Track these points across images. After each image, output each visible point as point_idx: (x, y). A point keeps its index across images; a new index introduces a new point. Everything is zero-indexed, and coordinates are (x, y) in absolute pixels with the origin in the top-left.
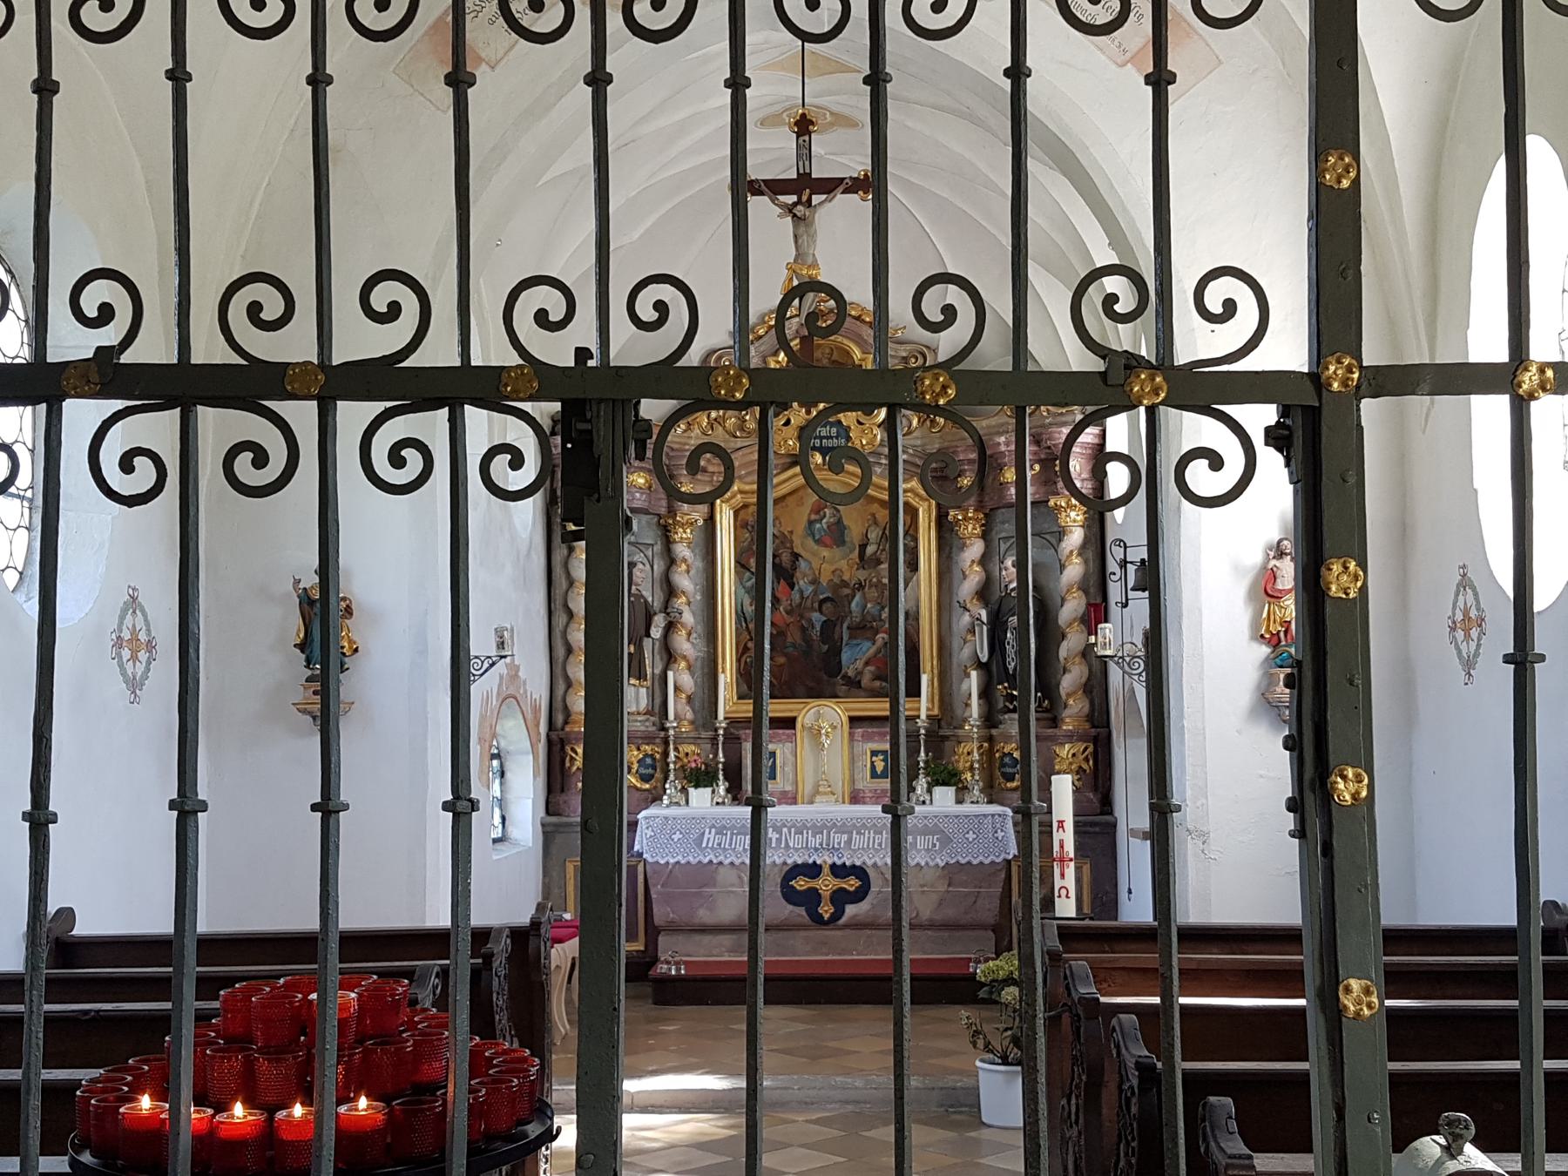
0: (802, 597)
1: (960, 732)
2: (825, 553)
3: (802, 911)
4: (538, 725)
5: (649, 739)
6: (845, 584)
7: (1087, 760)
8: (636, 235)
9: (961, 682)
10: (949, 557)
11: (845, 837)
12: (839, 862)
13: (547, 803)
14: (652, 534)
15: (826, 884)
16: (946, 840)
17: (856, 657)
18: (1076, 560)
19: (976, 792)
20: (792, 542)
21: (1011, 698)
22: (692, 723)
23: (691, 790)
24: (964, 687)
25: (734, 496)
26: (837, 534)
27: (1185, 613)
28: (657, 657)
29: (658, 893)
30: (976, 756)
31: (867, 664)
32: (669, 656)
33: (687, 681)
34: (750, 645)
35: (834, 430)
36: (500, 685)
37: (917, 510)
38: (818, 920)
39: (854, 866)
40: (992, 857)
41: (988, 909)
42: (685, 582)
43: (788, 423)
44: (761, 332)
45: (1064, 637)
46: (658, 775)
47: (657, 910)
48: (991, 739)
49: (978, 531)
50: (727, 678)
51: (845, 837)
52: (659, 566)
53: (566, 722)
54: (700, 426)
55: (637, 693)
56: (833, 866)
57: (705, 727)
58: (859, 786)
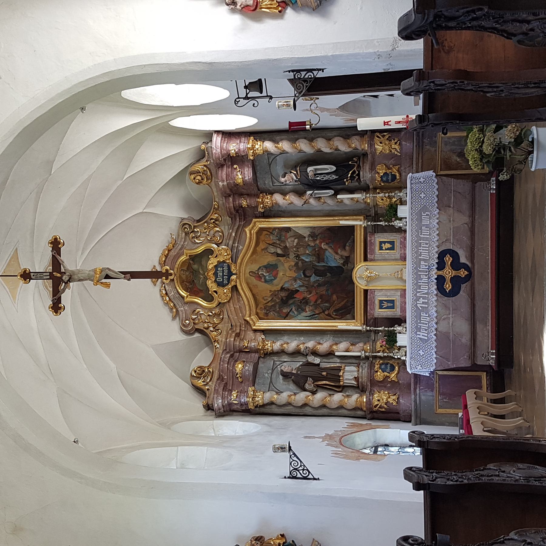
1: (371, 204)
2: (281, 274)
3: (463, 286)
4: (361, 425)
5: (372, 366)
6: (296, 264)
7: (383, 136)
8: (113, 365)
9: (345, 204)
10: (284, 212)
11: (422, 263)
12: (436, 266)
13: (405, 421)
14: (268, 362)
15: (448, 273)
16: (425, 209)
17: (333, 259)
19: (401, 194)
20: (275, 291)
21: (352, 178)
23: (398, 344)
24: (347, 202)
25: (253, 321)
26: (272, 268)
27: (267, 57)
28: (331, 360)
31: (337, 253)
32: (330, 354)
33: (343, 345)
34: (326, 313)
35: (219, 269)
38: (469, 277)
39: (438, 258)
41: (464, 186)
42: (292, 345)
43: (216, 292)
44: (172, 304)
45: (319, 151)
46: (391, 362)
47: (463, 365)
48: (375, 189)
50: (342, 325)
51: (422, 263)
52: (285, 358)
53: (362, 410)
56: (438, 269)
57: (369, 337)
58: (398, 256)
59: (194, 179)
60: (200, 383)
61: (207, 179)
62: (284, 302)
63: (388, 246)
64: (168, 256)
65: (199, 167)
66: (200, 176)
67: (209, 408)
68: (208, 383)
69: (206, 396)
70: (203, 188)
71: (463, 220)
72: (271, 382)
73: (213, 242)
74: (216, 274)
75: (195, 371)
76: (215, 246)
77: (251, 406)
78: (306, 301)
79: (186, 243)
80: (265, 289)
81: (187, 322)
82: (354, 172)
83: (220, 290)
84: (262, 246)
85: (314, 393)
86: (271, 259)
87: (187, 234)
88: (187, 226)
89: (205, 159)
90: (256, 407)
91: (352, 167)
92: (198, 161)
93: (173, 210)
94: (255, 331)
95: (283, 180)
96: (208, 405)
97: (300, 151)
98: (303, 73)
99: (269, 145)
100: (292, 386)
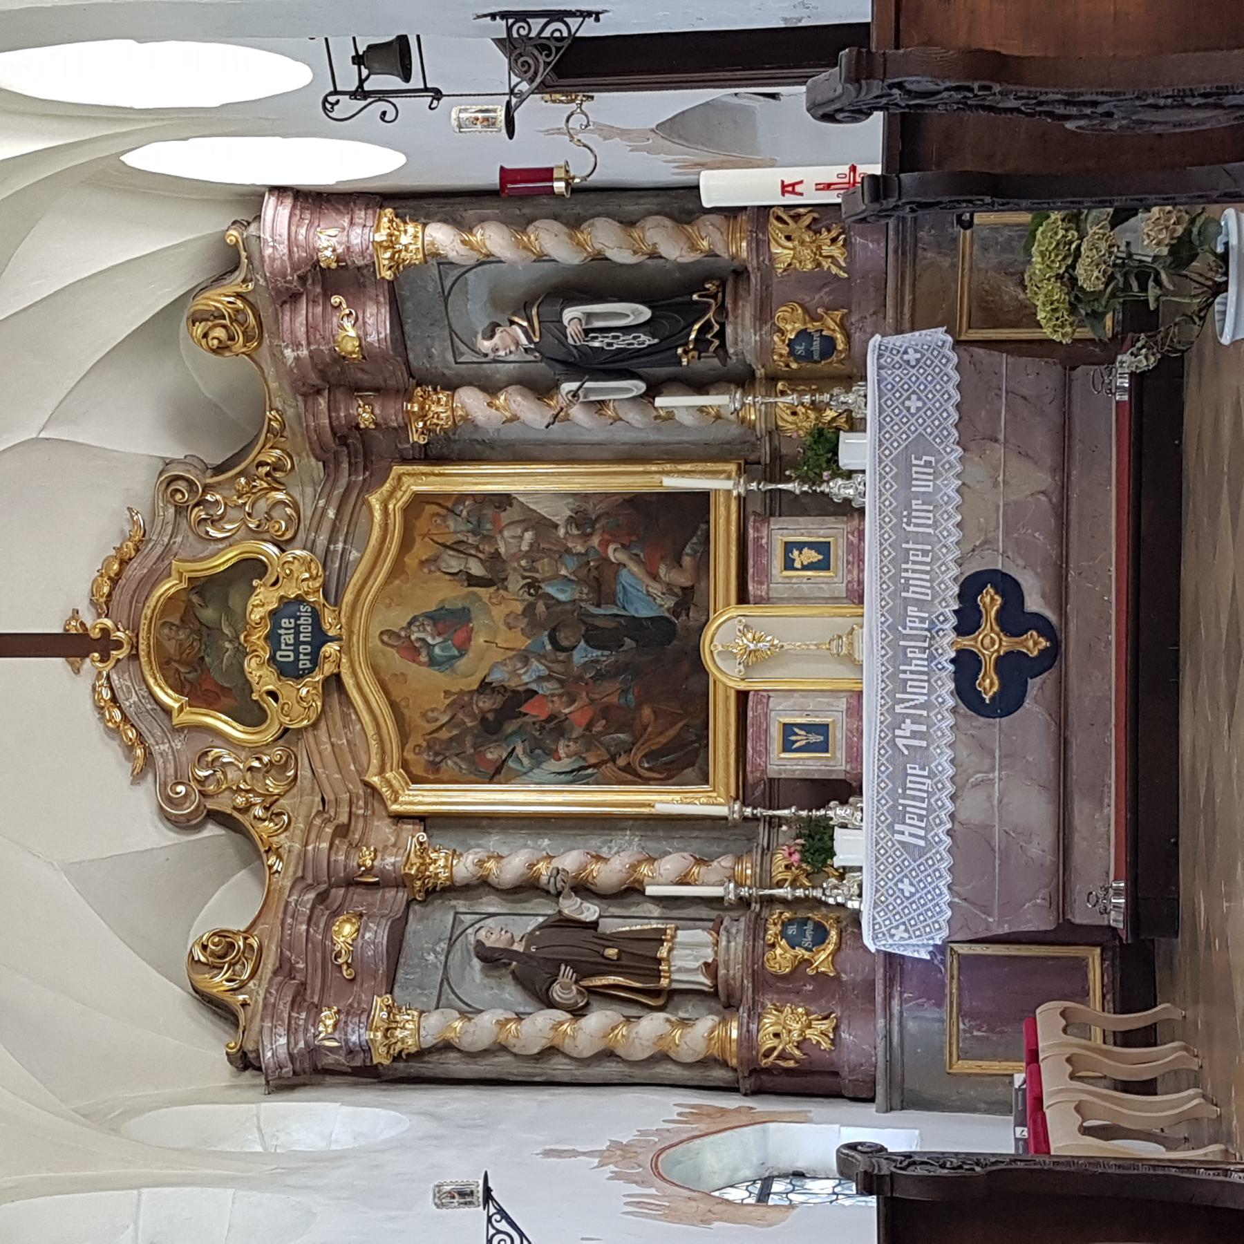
0: (548, 678)
1: (761, 427)
2: (479, 640)
3: (1034, 684)
4: (723, 1112)
5: (757, 928)
6: (529, 610)
11: (912, 611)
12: (953, 621)
14: (438, 915)
15: (990, 642)
16: (920, 445)
17: (644, 592)
18: (478, 236)
19: (850, 398)
20: (462, 693)
22: (739, 859)
23: (838, 861)
24: (687, 419)
26: (452, 621)
28: (634, 911)
29: (1000, 923)
30: (791, 398)
31: (655, 577)
32: (631, 891)
33: (671, 864)
34: (622, 762)
35: (285, 622)
36: (629, 1179)
37: (417, 495)
38: (1052, 657)
39: (960, 597)
40: (950, 369)
42: (514, 862)
45: (600, 258)
46: (816, 916)
48: (772, 379)
49: (443, 397)
50: (667, 800)
51: (912, 611)
52: (491, 904)
53: (724, 1064)
54: (275, 834)
55: (686, 945)
56: (960, 630)
58: (841, 589)
59: (205, 336)
60: (218, 983)
61: (248, 339)
62: (491, 728)
63: (811, 556)
64: (119, 580)
65: (220, 299)
66: (224, 326)
67: (245, 1061)
68: (243, 985)
69: (237, 1026)
70: (233, 366)
71: (1033, 481)
72: (445, 978)
73: (267, 536)
74: (273, 639)
75: (204, 947)
76: (272, 549)
77: (380, 1057)
78: (556, 727)
79: (179, 539)
80: (430, 688)
81: (181, 789)
82: (707, 327)
83: (287, 689)
84: (421, 550)
85: (578, 1013)
86: (448, 593)
87: (180, 510)
88: (181, 485)
89: (239, 275)
90: (397, 1058)
91: (703, 309)
92: (218, 280)
93: (135, 438)
94: (399, 818)
95: (485, 345)
96: (245, 1054)
97: (541, 258)
98: (537, 24)
99: (441, 236)
100: (512, 993)
